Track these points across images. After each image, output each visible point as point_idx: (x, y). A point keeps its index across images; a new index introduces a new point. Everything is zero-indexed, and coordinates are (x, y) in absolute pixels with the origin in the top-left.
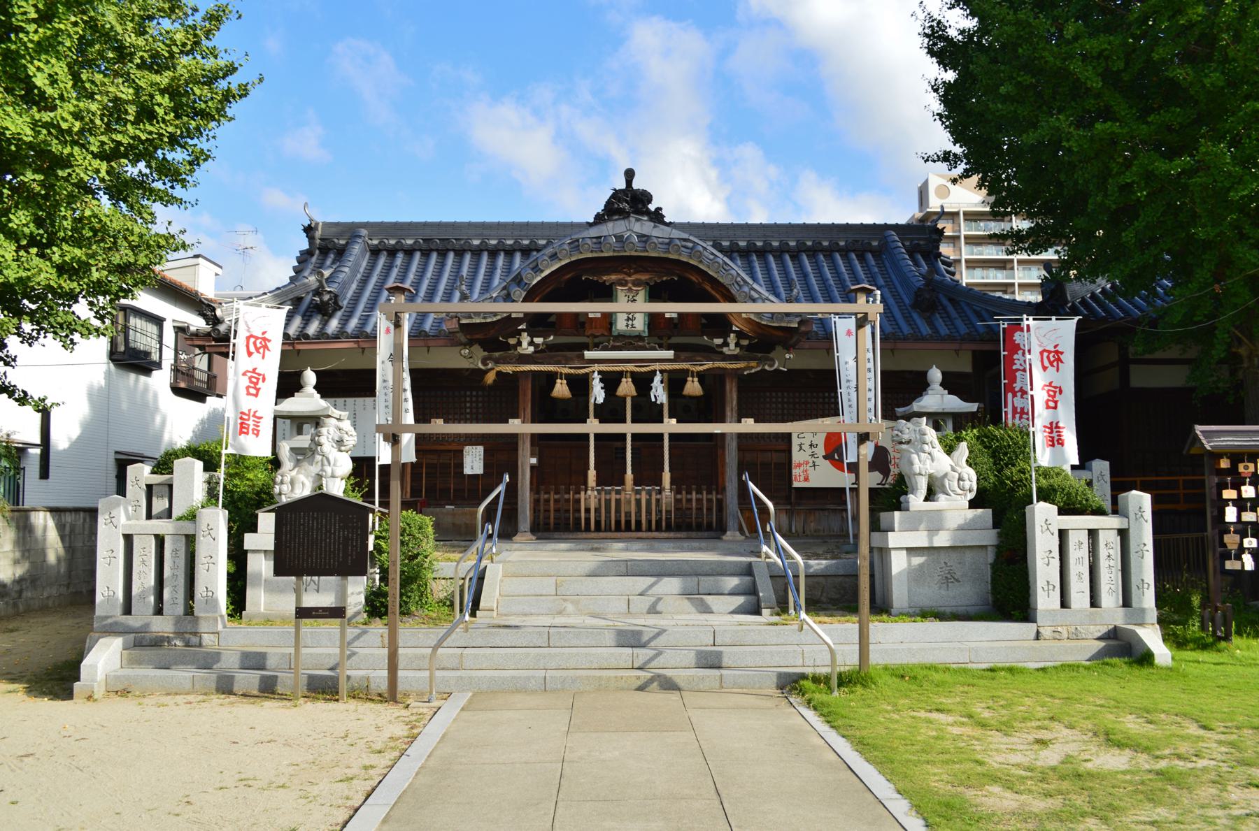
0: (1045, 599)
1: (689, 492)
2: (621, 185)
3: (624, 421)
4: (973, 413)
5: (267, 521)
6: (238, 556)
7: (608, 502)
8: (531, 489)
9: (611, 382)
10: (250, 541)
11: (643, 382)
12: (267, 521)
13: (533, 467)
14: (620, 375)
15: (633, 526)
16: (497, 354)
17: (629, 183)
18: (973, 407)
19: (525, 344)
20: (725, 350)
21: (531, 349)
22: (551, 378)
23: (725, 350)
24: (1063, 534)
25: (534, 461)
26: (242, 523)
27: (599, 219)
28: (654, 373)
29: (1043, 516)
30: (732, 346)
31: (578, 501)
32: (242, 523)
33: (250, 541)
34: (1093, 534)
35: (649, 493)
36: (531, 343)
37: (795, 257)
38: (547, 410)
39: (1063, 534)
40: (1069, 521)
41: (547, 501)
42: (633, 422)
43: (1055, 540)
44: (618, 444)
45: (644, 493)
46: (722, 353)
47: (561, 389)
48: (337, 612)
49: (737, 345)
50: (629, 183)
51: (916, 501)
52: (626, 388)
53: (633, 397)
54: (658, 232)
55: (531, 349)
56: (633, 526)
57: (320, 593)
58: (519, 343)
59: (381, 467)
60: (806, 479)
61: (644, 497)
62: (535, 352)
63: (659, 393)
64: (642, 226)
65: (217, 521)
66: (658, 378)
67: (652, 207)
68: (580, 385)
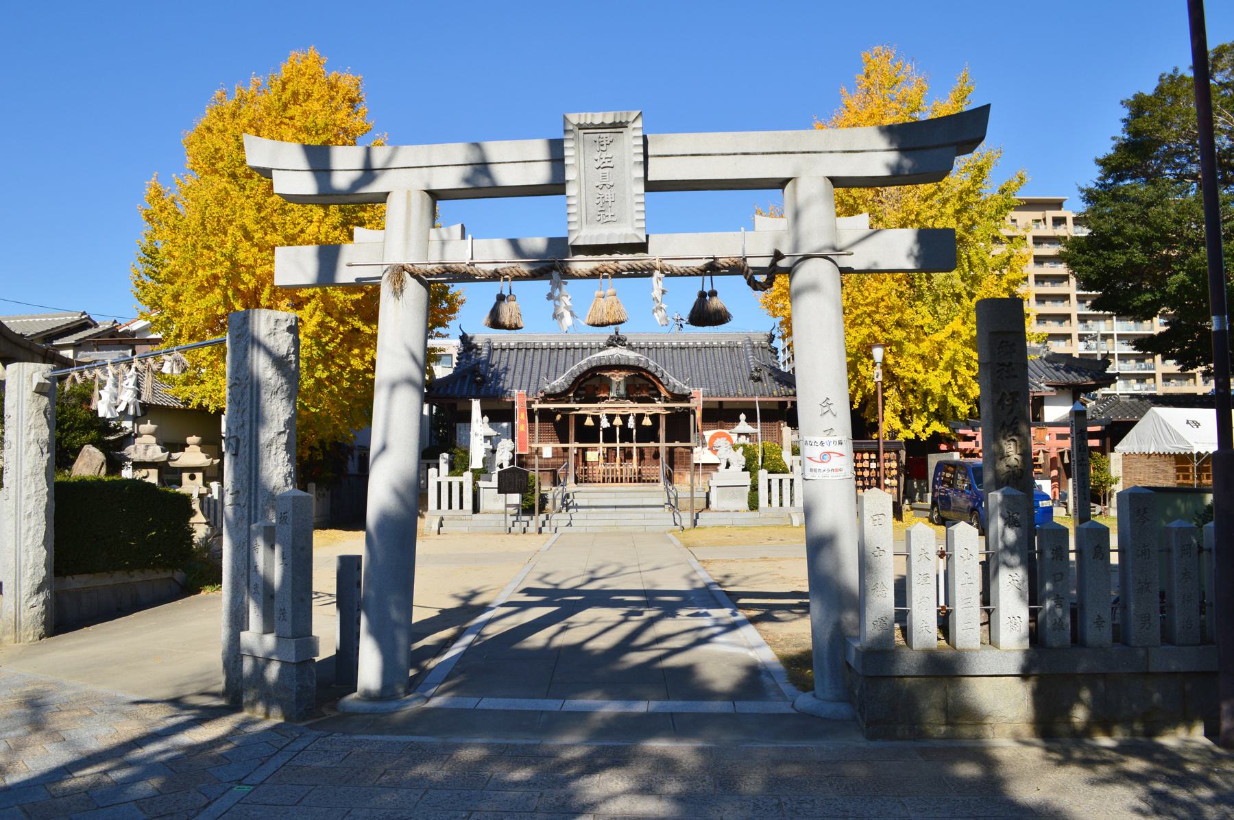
0: (763, 502)
9: (611, 418)
11: (625, 418)
14: (614, 416)
22: (585, 416)
29: (763, 475)
34: (781, 481)
40: (771, 476)
47: (589, 422)
51: (722, 468)
52: (618, 422)
63: (631, 424)
68: (596, 419)
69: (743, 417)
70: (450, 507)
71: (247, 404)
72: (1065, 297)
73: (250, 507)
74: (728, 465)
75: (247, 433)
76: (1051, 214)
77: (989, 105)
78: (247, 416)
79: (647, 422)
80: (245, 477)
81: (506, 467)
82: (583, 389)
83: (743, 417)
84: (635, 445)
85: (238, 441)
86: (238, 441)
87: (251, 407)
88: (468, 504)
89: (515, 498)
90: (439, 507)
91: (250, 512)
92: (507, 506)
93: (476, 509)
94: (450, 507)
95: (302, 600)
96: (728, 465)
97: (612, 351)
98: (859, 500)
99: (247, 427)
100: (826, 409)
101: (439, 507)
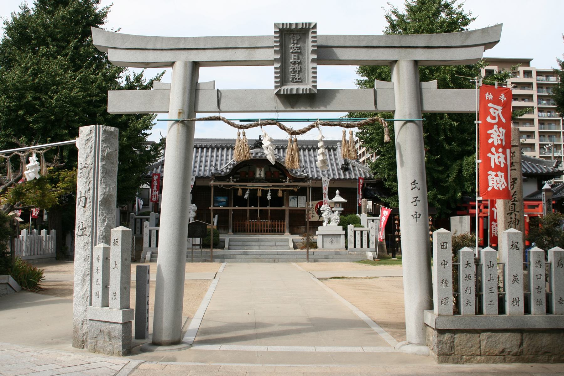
0: (351, 246)
18: (346, 201)
24: (355, 232)
34: (362, 232)
37: (309, 150)
39: (355, 232)
40: (356, 229)
51: (325, 224)
69: (337, 192)
71: (92, 179)
72: (530, 97)
73: (92, 237)
75: (91, 195)
76: (521, 69)
77: (501, 25)
78: (91, 186)
80: (90, 219)
81: (191, 222)
82: (238, 174)
83: (337, 192)
84: (259, 208)
85: (86, 199)
86: (86, 199)
87: (94, 180)
89: (198, 241)
91: (92, 239)
92: (193, 245)
95: (125, 288)
98: (210, 336)
99: (91, 191)
100: (414, 186)
101: (150, 246)
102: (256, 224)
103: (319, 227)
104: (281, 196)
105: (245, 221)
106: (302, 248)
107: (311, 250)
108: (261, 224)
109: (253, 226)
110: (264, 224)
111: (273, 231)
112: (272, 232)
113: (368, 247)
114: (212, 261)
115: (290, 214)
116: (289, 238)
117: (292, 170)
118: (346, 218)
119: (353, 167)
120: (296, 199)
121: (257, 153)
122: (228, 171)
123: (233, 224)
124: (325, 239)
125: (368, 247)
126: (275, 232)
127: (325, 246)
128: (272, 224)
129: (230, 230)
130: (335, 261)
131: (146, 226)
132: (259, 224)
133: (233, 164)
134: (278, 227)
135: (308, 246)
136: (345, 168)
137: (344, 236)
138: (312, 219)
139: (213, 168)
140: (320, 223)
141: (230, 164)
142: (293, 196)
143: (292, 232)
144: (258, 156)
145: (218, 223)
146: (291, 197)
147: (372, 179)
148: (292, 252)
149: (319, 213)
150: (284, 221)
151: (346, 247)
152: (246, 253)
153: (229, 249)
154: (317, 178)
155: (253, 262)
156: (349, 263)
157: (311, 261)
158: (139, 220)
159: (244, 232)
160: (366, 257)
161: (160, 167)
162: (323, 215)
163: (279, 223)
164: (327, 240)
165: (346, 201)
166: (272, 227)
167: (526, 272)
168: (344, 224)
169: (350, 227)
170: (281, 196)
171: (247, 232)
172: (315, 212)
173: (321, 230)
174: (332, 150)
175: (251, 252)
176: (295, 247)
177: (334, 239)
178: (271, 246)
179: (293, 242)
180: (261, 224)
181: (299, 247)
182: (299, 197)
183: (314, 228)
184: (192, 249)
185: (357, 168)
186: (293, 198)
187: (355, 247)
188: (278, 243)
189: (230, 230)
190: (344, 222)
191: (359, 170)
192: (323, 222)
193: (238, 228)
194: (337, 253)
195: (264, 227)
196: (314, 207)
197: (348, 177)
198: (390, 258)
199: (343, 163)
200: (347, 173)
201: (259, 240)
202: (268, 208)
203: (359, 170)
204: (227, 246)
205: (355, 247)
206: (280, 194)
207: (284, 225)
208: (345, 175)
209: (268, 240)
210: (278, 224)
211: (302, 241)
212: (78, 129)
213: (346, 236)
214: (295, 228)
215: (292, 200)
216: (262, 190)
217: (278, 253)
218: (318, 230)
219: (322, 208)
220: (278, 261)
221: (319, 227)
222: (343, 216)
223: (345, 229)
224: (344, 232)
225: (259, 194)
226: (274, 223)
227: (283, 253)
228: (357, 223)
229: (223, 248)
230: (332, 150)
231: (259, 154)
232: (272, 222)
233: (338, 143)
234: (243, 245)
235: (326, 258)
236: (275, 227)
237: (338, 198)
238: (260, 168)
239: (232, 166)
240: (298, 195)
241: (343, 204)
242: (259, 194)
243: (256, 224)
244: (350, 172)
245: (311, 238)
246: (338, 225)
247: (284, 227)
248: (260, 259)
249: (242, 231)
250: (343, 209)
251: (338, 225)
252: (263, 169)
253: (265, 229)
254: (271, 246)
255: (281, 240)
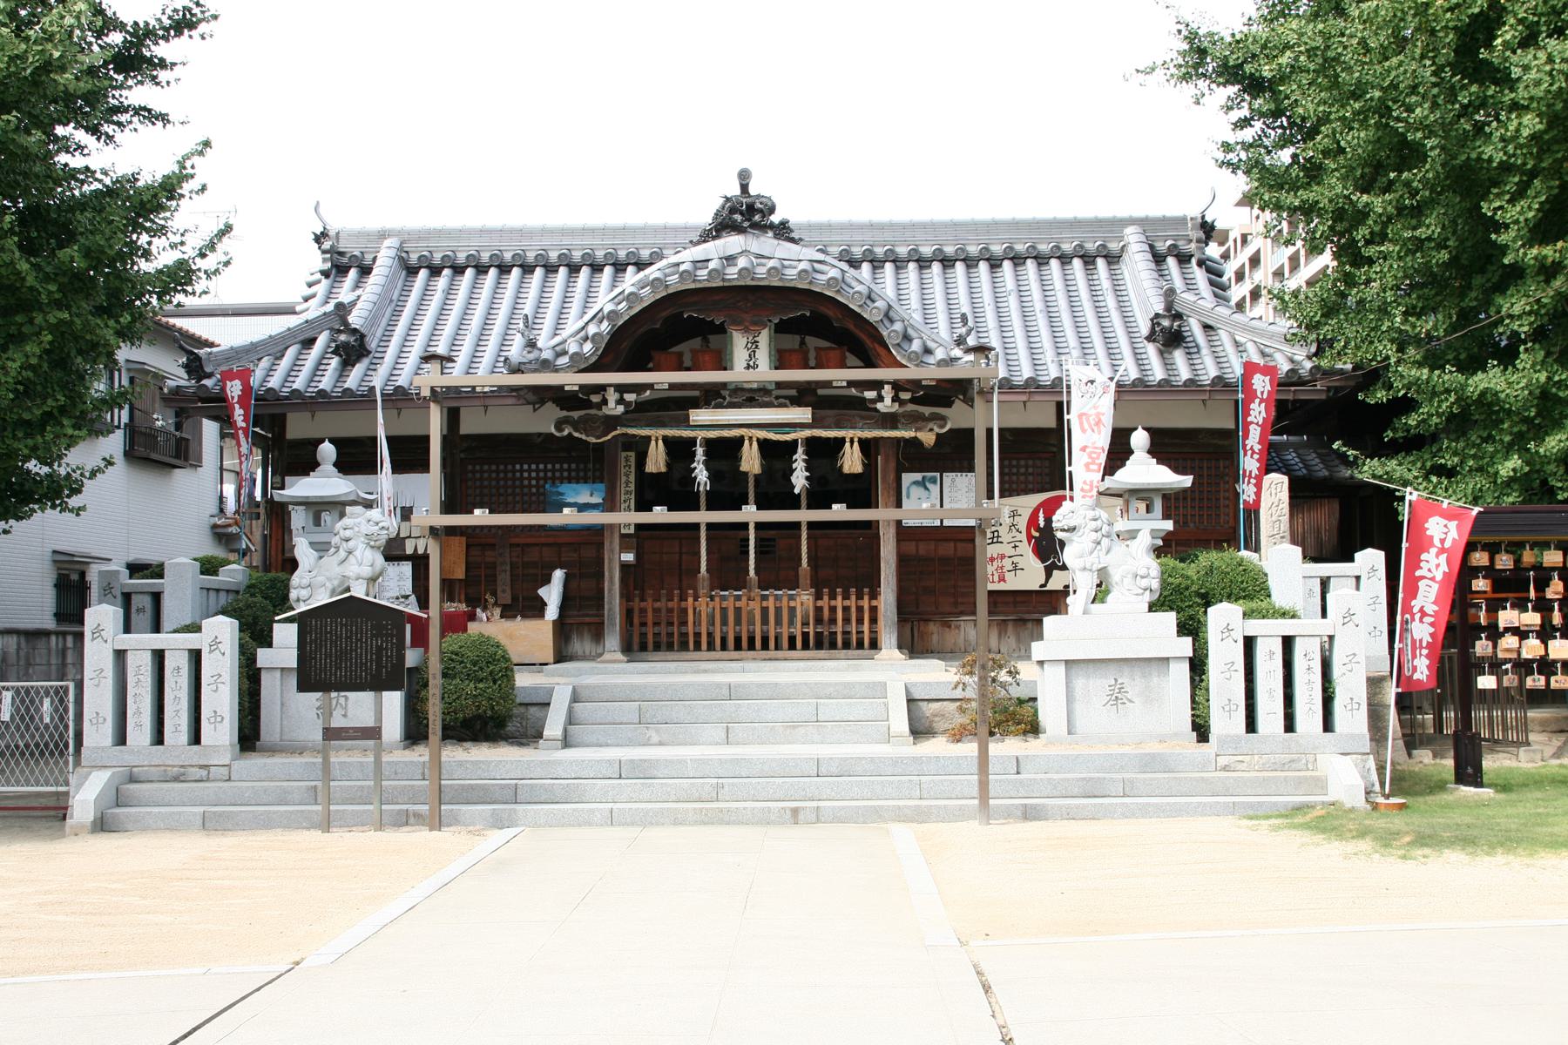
0: (1226, 718)
1: (833, 597)
2: (735, 190)
3: (698, 509)
4: (1185, 490)
5: (285, 635)
6: (250, 678)
7: (724, 611)
8: (622, 596)
10: (264, 657)
12: (285, 635)
13: (625, 567)
15: (745, 643)
16: (576, 414)
17: (744, 188)
18: (1186, 481)
19: (612, 404)
20: (879, 406)
21: (621, 409)
23: (879, 406)
24: (1249, 643)
25: (629, 557)
26: (256, 634)
27: (708, 235)
28: (795, 441)
30: (888, 401)
31: (685, 611)
32: (256, 634)
33: (264, 657)
34: (1288, 642)
35: (777, 598)
36: (620, 401)
37: (995, 264)
38: (650, 492)
39: (1249, 643)
40: (1255, 627)
41: (643, 611)
42: (708, 509)
43: (1240, 648)
44: (742, 534)
45: (771, 599)
46: (876, 410)
48: (373, 733)
49: (895, 399)
50: (744, 188)
53: (756, 476)
54: (785, 250)
55: (621, 409)
56: (745, 643)
57: (357, 707)
58: (605, 402)
59: (424, 467)
60: (1002, 579)
61: (771, 603)
62: (626, 412)
64: (765, 243)
65: (222, 632)
66: (800, 456)
67: (775, 219)
69: (327, 450)
70: (159, 738)
74: (1101, 592)
79: (852, 461)
88: (221, 727)
90: (121, 739)
93: (249, 737)
94: (159, 738)
96: (1101, 592)
97: (732, 243)
101: (121, 739)
102: (738, 610)
103: (1048, 621)
104: (858, 469)
105: (683, 598)
106: (958, 736)
107: (1005, 748)
108: (765, 611)
109: (724, 622)
110: (778, 610)
111: (822, 640)
112: (819, 645)
113: (1328, 726)
114: (436, 822)
115: (903, 561)
116: (893, 672)
117: (907, 338)
118: (1191, 570)
119: (1207, 328)
120: (935, 489)
121: (730, 259)
122: (588, 347)
123: (628, 615)
124: (1080, 683)
125: (1328, 726)
126: (833, 646)
127: (1080, 723)
128: (819, 610)
129: (613, 641)
130: (1144, 812)
131: (98, 631)
132: (756, 606)
133: (612, 315)
134: (847, 620)
135: (984, 730)
136: (1170, 337)
137: (1185, 667)
138: (1014, 583)
139: (518, 342)
140: (1053, 601)
141: (598, 318)
142: (918, 476)
143: (914, 647)
144: (732, 272)
145: (563, 608)
146: (908, 478)
147: (1302, 382)
148: (896, 761)
149: (1048, 547)
150: (874, 595)
151: (1201, 731)
152: (642, 772)
153: (566, 742)
154: (1031, 382)
155: (677, 822)
156: (1229, 827)
157: (1007, 814)
158: (146, 602)
159: (684, 646)
160: (1321, 784)
161: (291, 352)
162: (1068, 556)
163: (852, 603)
164: (1094, 687)
165: (1186, 481)
166: (819, 620)
167: (874, 603)
168: (1185, 605)
169: (1224, 619)
170: (858, 469)
171: (698, 647)
172: (1026, 549)
173: (1059, 635)
174: (1100, 262)
175: (669, 762)
176: (920, 730)
177: (1133, 684)
178: (793, 724)
179: (910, 701)
180: (765, 611)
181: (940, 725)
182: (948, 477)
183: (1021, 622)
184: (325, 754)
185: (1223, 335)
186: (922, 484)
187: (1251, 726)
188: (830, 708)
189: (613, 641)
190: (1178, 590)
191: (1237, 344)
192: (1065, 592)
193: (650, 630)
194: (1150, 763)
195: (778, 622)
196: (1022, 523)
197: (1185, 374)
198: (1440, 786)
199: (1159, 308)
200: (1178, 356)
201: (732, 693)
202: (750, 513)
203: (1237, 344)
204: (554, 726)
205: (1251, 726)
206: (852, 461)
207: (874, 610)
208: (1168, 365)
209: (775, 693)
210: (846, 609)
211: (958, 694)
212: (652, 474)
213: (1198, 666)
214: (933, 627)
215: (917, 492)
216: (764, 445)
217: (819, 770)
218: (1040, 637)
219: (1060, 518)
220: (819, 817)
221: (1048, 621)
222: (1171, 562)
223: (1191, 628)
224: (1185, 646)
225: (751, 461)
226: (824, 603)
227: (845, 769)
228: (1251, 591)
229: (530, 735)
230: (1100, 262)
231: (742, 262)
232: (818, 597)
233: (1129, 230)
234: (647, 717)
235: (1093, 792)
236: (833, 621)
237: (1144, 470)
238: (751, 327)
239: (605, 326)
240: (942, 470)
241: (1172, 502)
242: (751, 461)
243: (738, 610)
244: (1192, 352)
245: (1003, 676)
246: (1153, 607)
247: (874, 620)
248: (712, 802)
249: (670, 647)
250: (1169, 525)
251: (1153, 607)
252: (764, 338)
253: (785, 631)
254: (793, 724)
255: (846, 692)
